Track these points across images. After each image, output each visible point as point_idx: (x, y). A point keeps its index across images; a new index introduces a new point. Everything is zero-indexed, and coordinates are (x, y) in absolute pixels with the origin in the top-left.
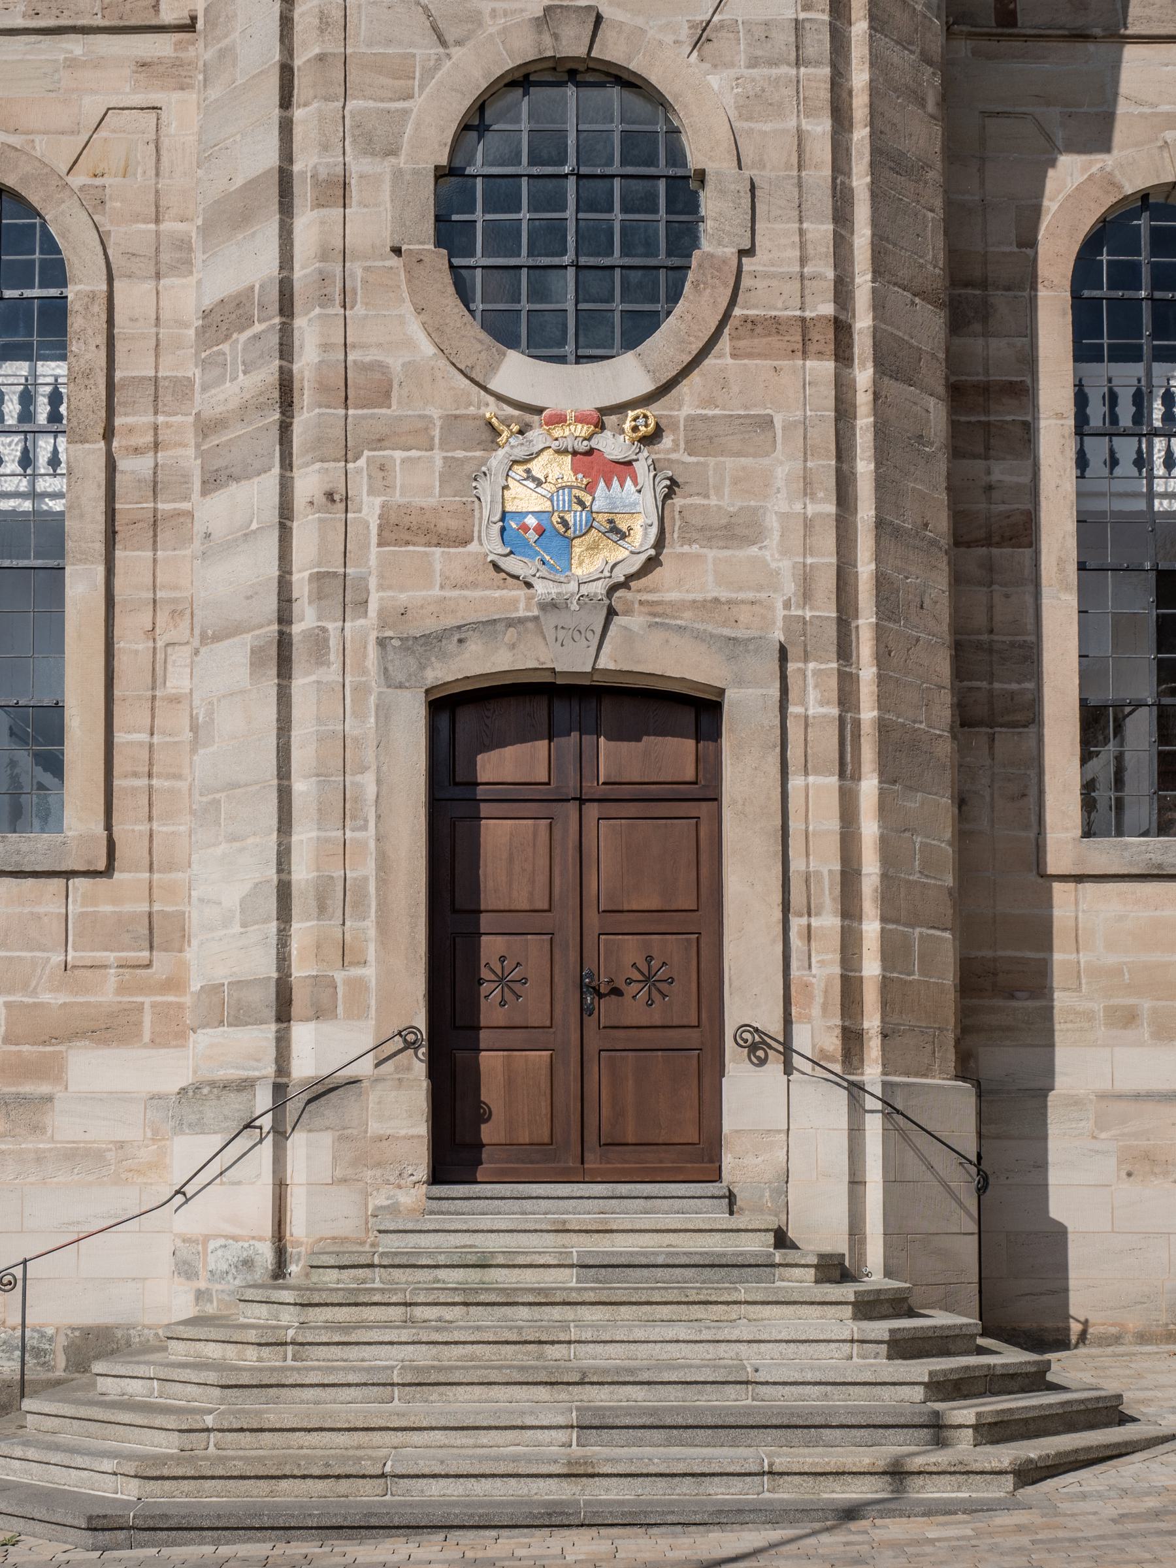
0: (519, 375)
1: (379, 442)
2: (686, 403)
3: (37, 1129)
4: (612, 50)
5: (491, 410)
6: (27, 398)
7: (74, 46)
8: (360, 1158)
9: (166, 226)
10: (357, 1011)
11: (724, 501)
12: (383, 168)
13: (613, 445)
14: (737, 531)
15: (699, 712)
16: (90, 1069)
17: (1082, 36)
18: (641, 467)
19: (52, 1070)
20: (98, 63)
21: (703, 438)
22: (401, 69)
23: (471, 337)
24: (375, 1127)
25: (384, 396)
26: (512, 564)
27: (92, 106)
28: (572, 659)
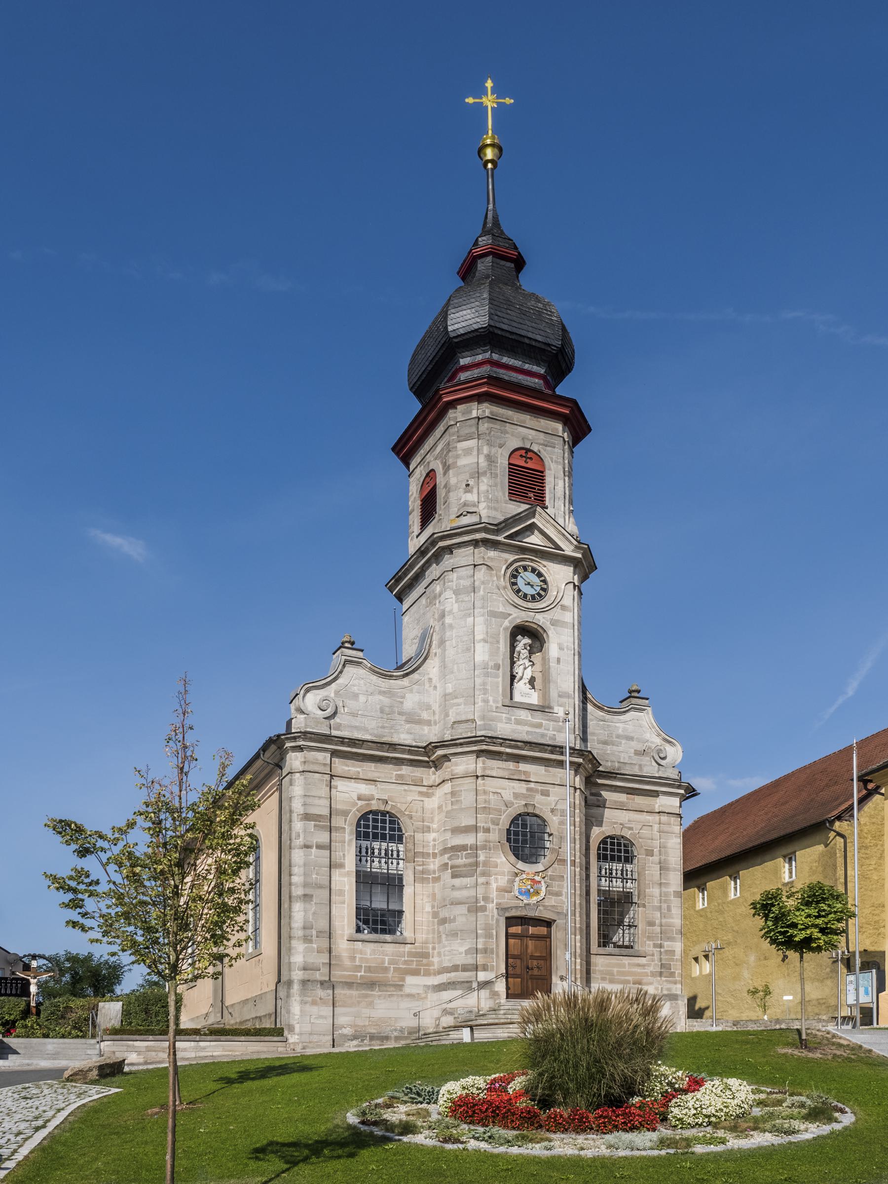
0: (521, 865)
1: (496, 874)
2: (550, 872)
3: (401, 990)
4: (537, 812)
5: (516, 871)
6: (380, 850)
7: (406, 787)
8: (495, 995)
9: (425, 823)
10: (492, 970)
11: (555, 889)
12: (497, 827)
13: (537, 878)
14: (558, 894)
15: (548, 924)
16: (410, 980)
17: (599, 806)
18: (543, 882)
19: (403, 980)
20: (411, 791)
21: (552, 878)
22: (499, 811)
23: (513, 858)
24: (496, 989)
25: (496, 866)
26: (520, 897)
27: (409, 799)
28: (531, 914)
